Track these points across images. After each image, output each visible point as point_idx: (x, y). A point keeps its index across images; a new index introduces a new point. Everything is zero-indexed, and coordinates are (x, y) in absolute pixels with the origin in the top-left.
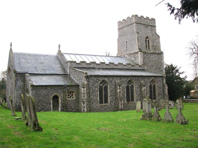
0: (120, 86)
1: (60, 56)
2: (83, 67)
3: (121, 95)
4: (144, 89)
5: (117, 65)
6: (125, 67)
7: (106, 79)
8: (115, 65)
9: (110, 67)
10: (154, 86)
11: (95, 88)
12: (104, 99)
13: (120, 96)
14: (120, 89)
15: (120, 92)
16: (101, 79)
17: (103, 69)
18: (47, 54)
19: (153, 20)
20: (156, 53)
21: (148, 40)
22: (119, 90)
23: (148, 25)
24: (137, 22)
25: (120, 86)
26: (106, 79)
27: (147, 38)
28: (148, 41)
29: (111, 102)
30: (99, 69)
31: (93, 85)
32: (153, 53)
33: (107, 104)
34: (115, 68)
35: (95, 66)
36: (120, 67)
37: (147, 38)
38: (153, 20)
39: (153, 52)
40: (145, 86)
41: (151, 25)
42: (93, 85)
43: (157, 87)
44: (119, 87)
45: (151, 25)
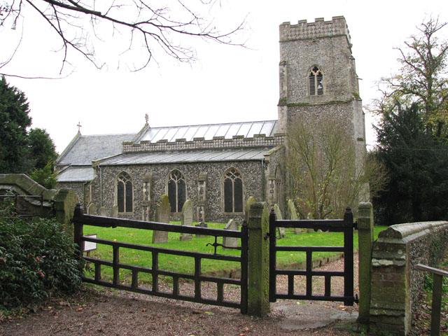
0: (146, 183)
1: (48, 135)
2: (143, 150)
3: (149, 199)
4: (201, 188)
5: (211, 142)
6: (230, 145)
7: (128, 171)
8: (187, 143)
9: (194, 148)
10: (239, 183)
11: (110, 186)
12: (177, 202)
13: (147, 199)
14: (146, 187)
15: (146, 193)
16: (227, 167)
17: (180, 151)
18: (125, 133)
19: (340, 20)
20: (340, 103)
21: (320, 73)
22: (144, 190)
23: (320, 38)
24: (285, 39)
25: (146, 183)
26: (128, 171)
27: (316, 69)
28: (320, 75)
29: (136, 210)
30: (172, 152)
31: (106, 181)
32: (332, 103)
33: (129, 213)
34: (204, 147)
35: (166, 147)
36: (216, 145)
37: (316, 69)
38: (340, 20)
39: (331, 99)
40: (203, 181)
41: (329, 34)
42: (106, 181)
43: (246, 184)
44: (144, 184)
45: (328, 37)
